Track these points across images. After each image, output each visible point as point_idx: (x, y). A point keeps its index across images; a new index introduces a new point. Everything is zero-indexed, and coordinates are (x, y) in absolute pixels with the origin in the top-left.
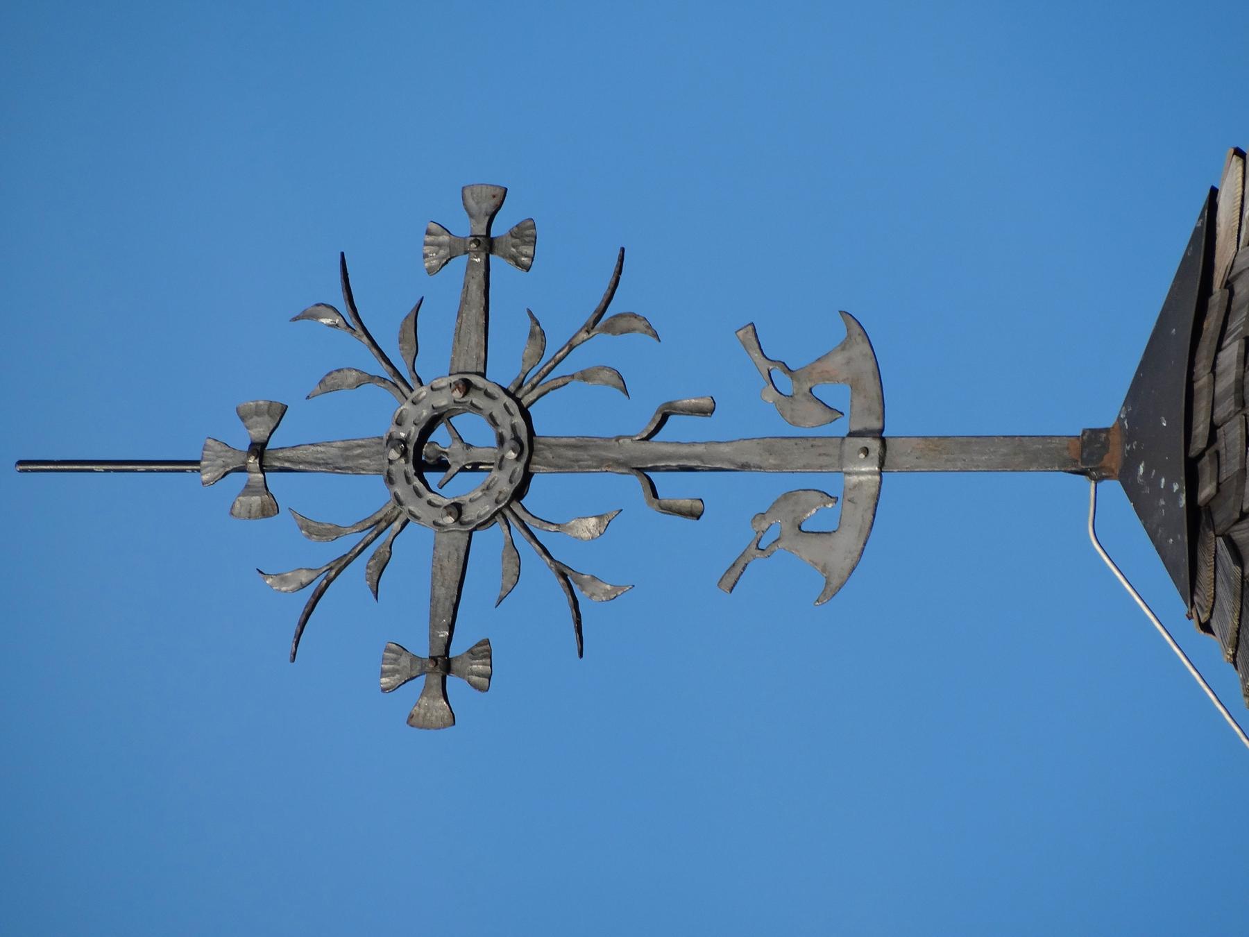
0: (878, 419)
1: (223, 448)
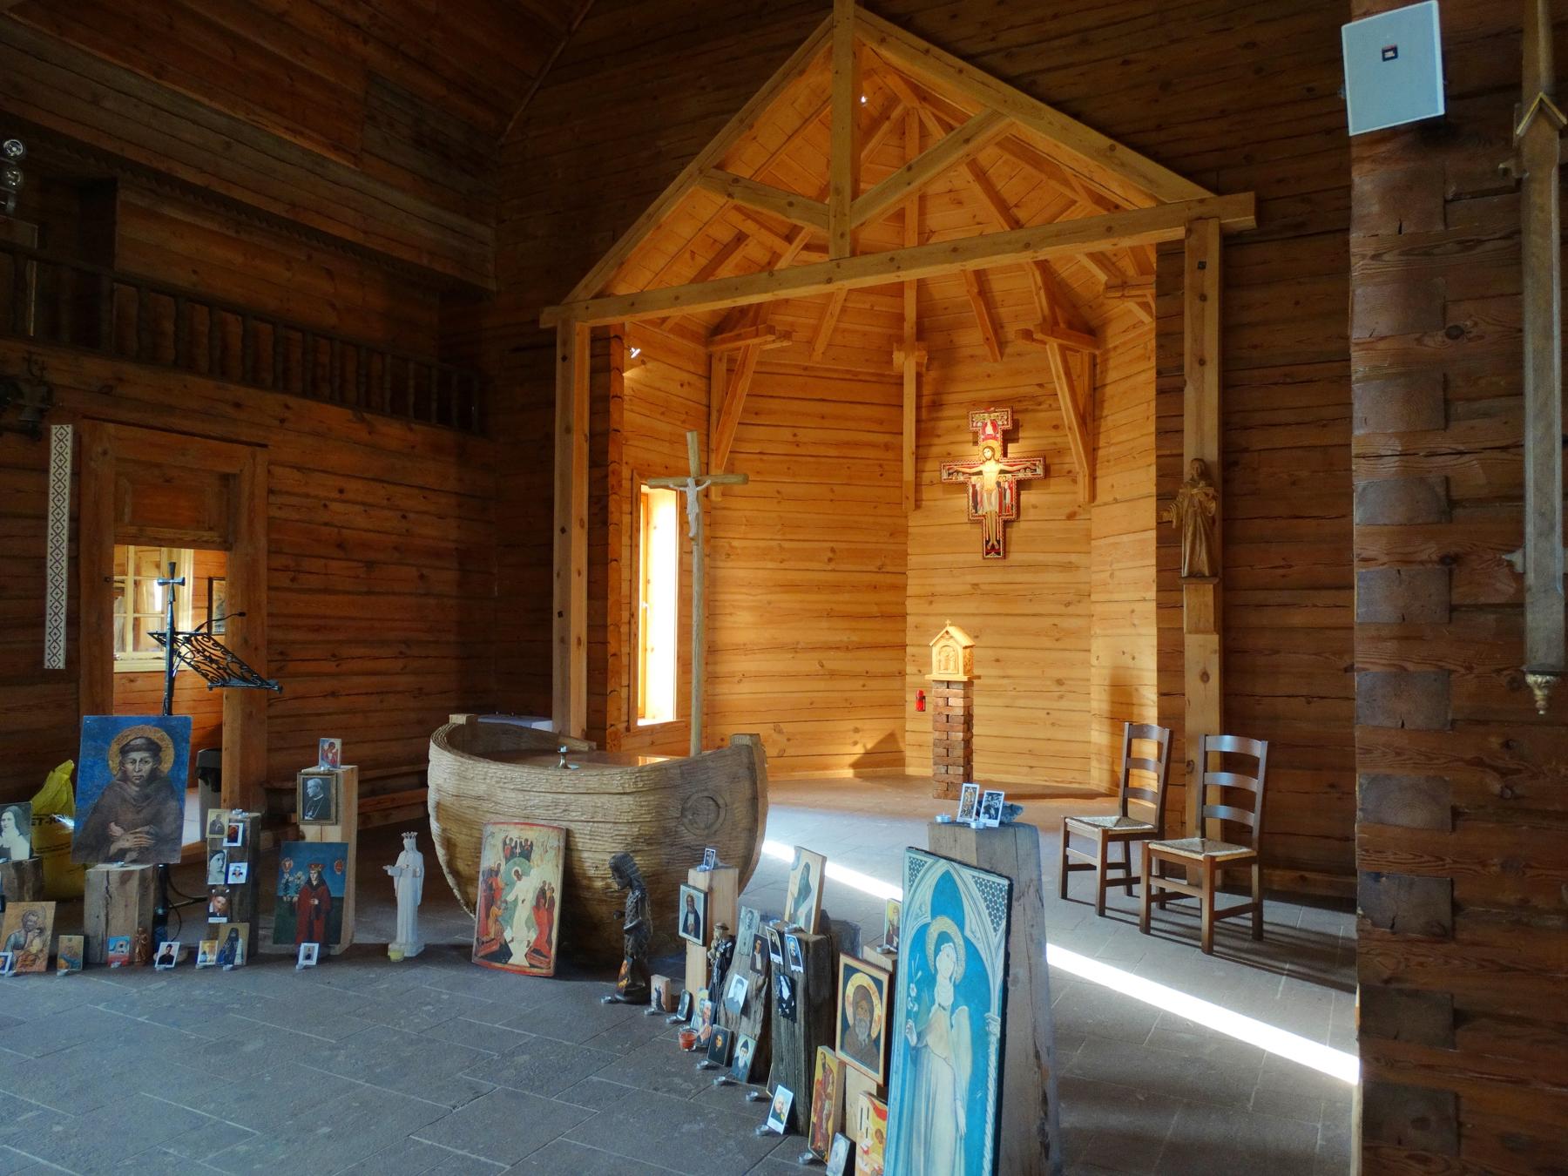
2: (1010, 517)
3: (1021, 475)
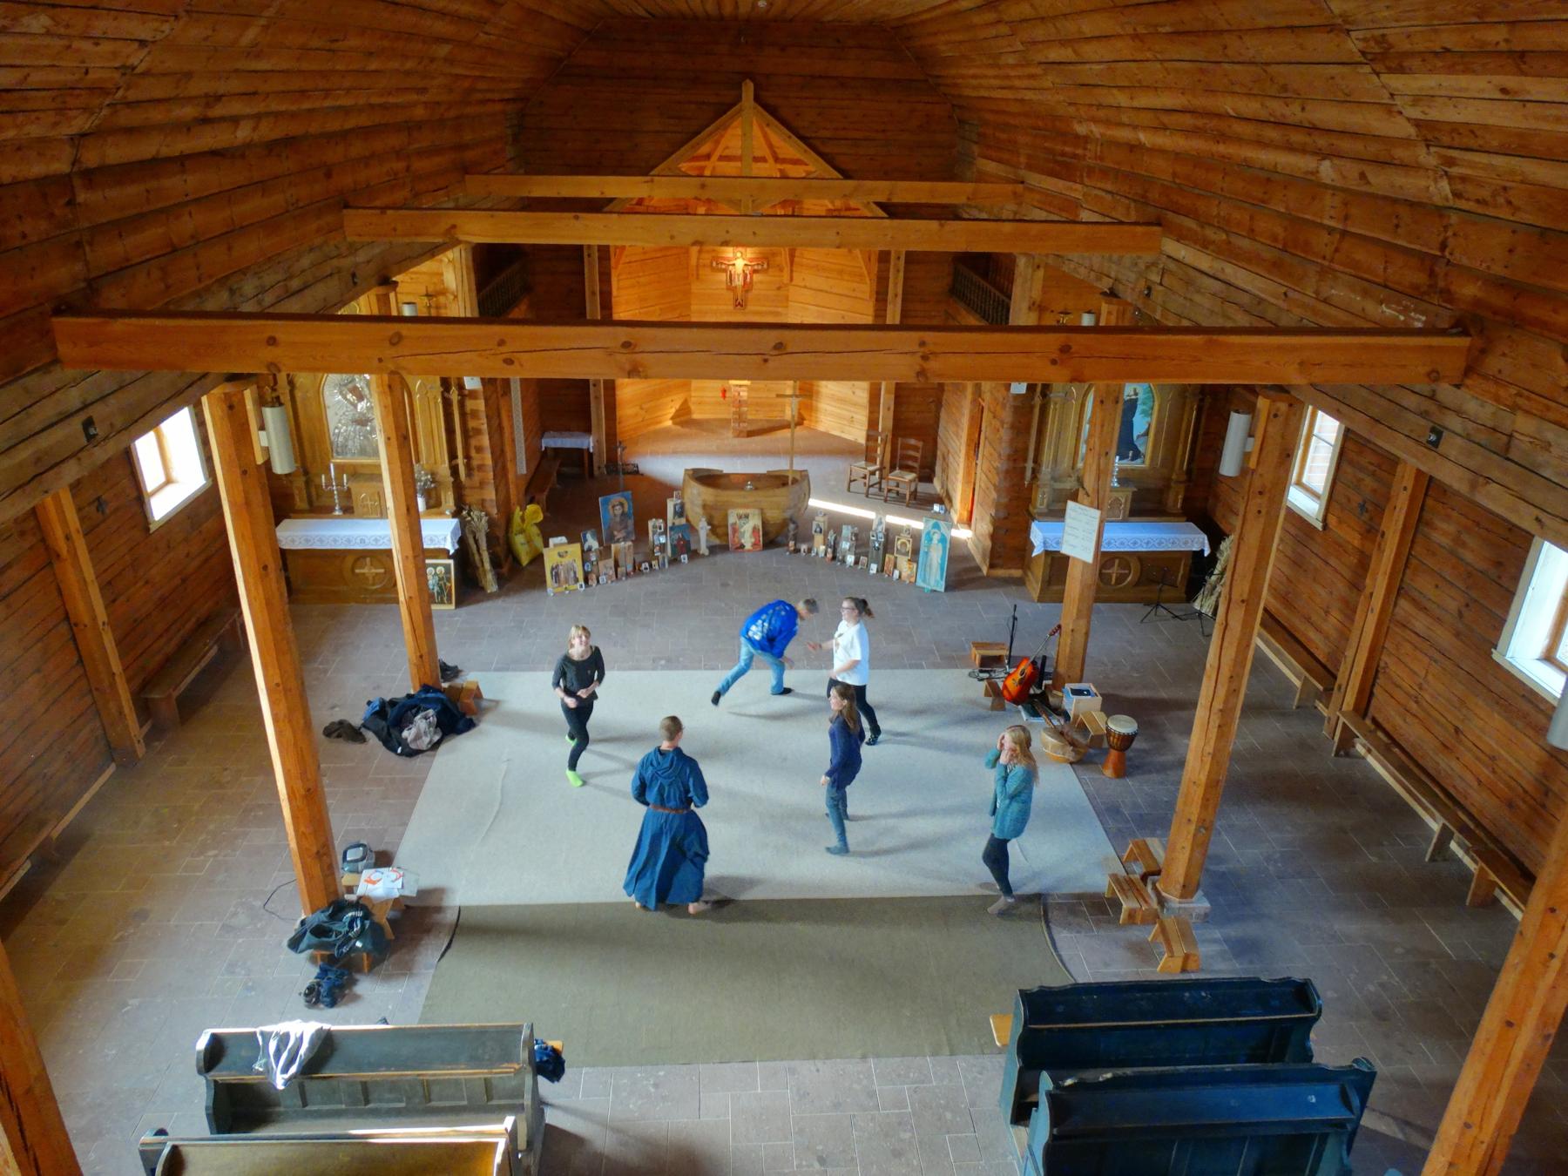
0: (1372, 386)
1: (648, 874)
2: (747, 286)
3: (756, 267)
